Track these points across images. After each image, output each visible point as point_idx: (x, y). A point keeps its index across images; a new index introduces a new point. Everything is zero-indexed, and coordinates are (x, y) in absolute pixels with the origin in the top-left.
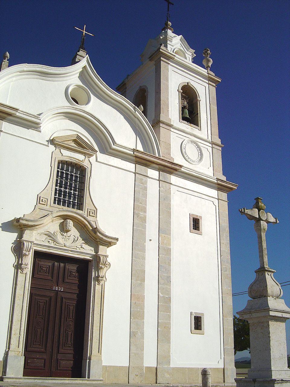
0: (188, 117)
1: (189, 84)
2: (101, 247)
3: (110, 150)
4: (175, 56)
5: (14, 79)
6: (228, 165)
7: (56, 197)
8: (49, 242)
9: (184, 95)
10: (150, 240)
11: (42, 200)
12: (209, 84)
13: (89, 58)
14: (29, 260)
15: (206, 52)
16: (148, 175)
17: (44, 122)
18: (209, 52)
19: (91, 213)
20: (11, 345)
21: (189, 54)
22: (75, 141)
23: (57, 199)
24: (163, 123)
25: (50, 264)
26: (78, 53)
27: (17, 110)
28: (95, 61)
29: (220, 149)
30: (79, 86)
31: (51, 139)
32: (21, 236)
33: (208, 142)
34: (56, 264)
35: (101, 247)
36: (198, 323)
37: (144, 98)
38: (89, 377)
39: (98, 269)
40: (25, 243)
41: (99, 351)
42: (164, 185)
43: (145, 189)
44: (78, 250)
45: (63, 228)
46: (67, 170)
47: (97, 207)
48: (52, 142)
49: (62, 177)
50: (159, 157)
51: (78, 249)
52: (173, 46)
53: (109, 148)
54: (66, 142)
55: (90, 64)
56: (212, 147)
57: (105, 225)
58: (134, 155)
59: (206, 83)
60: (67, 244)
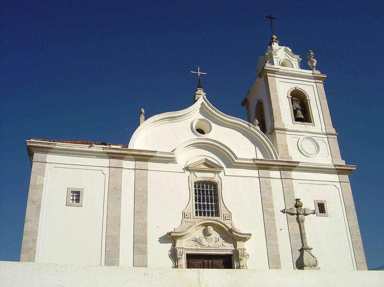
1: (297, 89)
2: (238, 243)
3: (234, 164)
5: (150, 128)
6: (346, 150)
7: (197, 210)
8: (196, 246)
9: (295, 98)
10: (281, 230)
11: (186, 215)
12: (316, 82)
15: (309, 54)
16: (271, 177)
17: (178, 155)
18: (312, 53)
19: (227, 217)
21: (294, 61)
22: (205, 164)
23: (198, 211)
24: (278, 129)
25: (201, 262)
26: (196, 93)
27: (155, 152)
29: (336, 137)
30: (200, 120)
31: (186, 166)
32: (174, 245)
33: (323, 134)
34: (205, 261)
35: (238, 243)
37: (259, 115)
39: (239, 260)
40: (178, 250)
42: (286, 182)
43: (270, 188)
44: (220, 248)
45: (206, 234)
46: (203, 187)
47: (231, 212)
48: (187, 169)
49: (199, 194)
50: (277, 160)
51: (220, 247)
52: (278, 58)
54: (199, 166)
55: (206, 100)
56: (327, 138)
57: (239, 225)
58: (255, 163)
59: (313, 82)
60: (211, 245)
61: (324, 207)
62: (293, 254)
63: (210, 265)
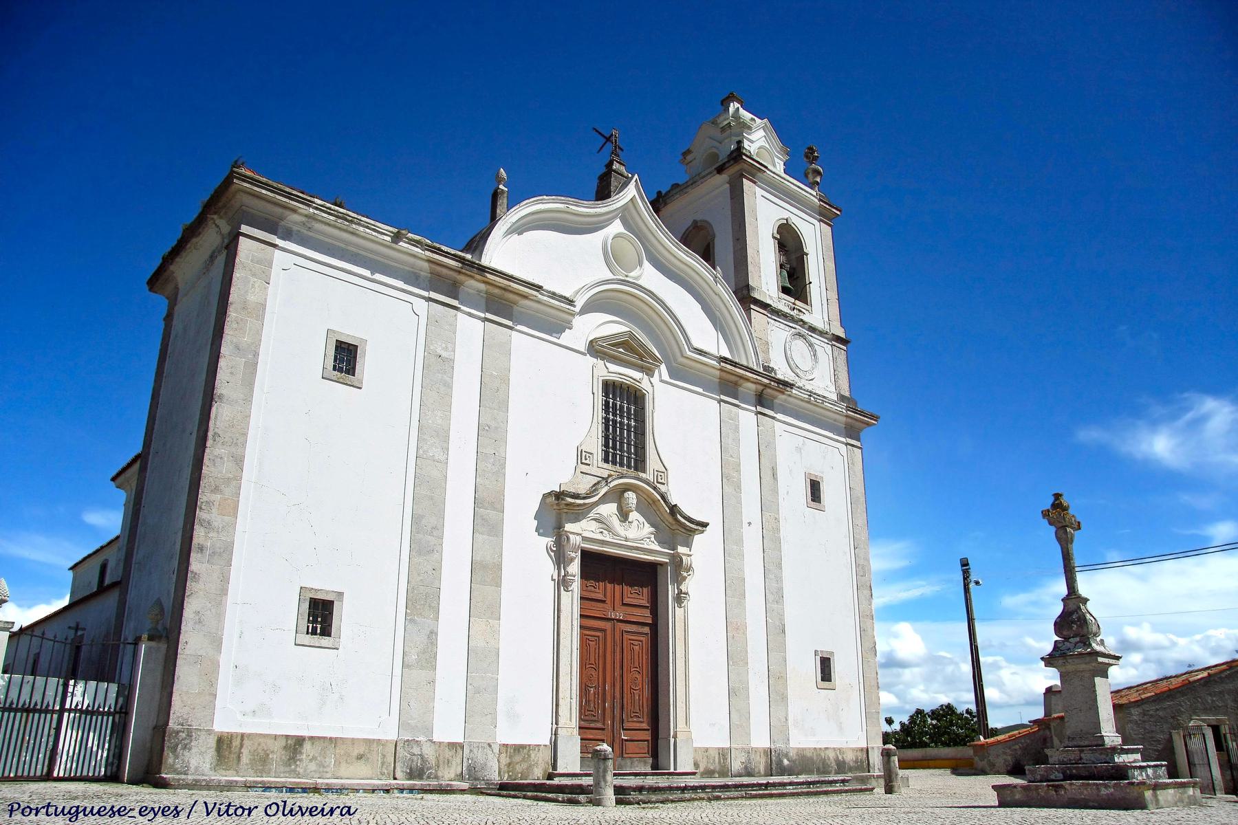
14: (575, 568)
27: (538, 288)
38: (905, 764)
39: (679, 579)
43: (736, 429)
53: (678, 354)
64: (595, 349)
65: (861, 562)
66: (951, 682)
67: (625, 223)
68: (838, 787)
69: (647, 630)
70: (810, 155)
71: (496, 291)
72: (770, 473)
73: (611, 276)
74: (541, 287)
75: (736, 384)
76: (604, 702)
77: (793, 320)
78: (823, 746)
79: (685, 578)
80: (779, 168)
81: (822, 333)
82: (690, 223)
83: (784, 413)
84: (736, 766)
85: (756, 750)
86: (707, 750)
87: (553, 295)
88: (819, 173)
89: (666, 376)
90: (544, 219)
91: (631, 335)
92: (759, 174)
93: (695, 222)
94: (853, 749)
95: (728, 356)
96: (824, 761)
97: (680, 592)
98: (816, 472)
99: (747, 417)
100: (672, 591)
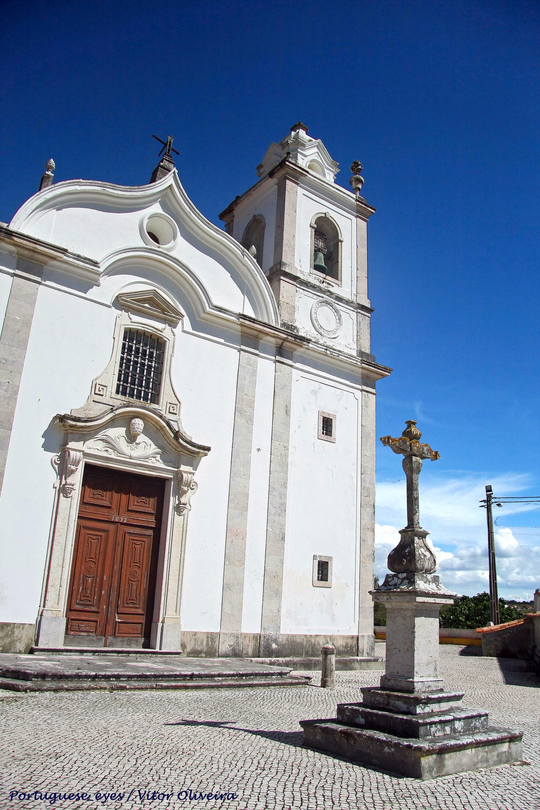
0: (323, 265)
1: (328, 216)
4: (307, 172)
10: (259, 450)
13: (177, 171)
14: (77, 479)
19: (171, 408)
20: (47, 602)
27: (64, 251)
28: (187, 181)
36: (323, 569)
37: (259, 235)
39: (180, 493)
41: (177, 609)
43: (254, 373)
47: (180, 400)
57: (192, 427)
58: (239, 323)
61: (331, 425)
62: (270, 496)
63: (92, 512)
64: (121, 303)
65: (367, 485)
66: (477, 582)
67: (164, 206)
68: (274, 680)
69: (150, 532)
70: (355, 168)
71: (26, 252)
72: (283, 410)
73: (143, 245)
74: (66, 250)
75: (257, 337)
76: (101, 590)
77: (320, 290)
78: (313, 633)
79: (185, 492)
80: (330, 178)
81: (348, 302)
82: (250, 218)
83: (303, 362)
84: (224, 647)
85: (245, 636)
86: (195, 634)
87: (78, 257)
88: (360, 181)
89: (188, 327)
90: (79, 199)
91: (156, 293)
92: (302, 178)
93: (255, 216)
94: (344, 637)
95: (252, 314)
96: (313, 646)
97: (180, 503)
98: (329, 411)
99: (265, 366)
100: (173, 501)
